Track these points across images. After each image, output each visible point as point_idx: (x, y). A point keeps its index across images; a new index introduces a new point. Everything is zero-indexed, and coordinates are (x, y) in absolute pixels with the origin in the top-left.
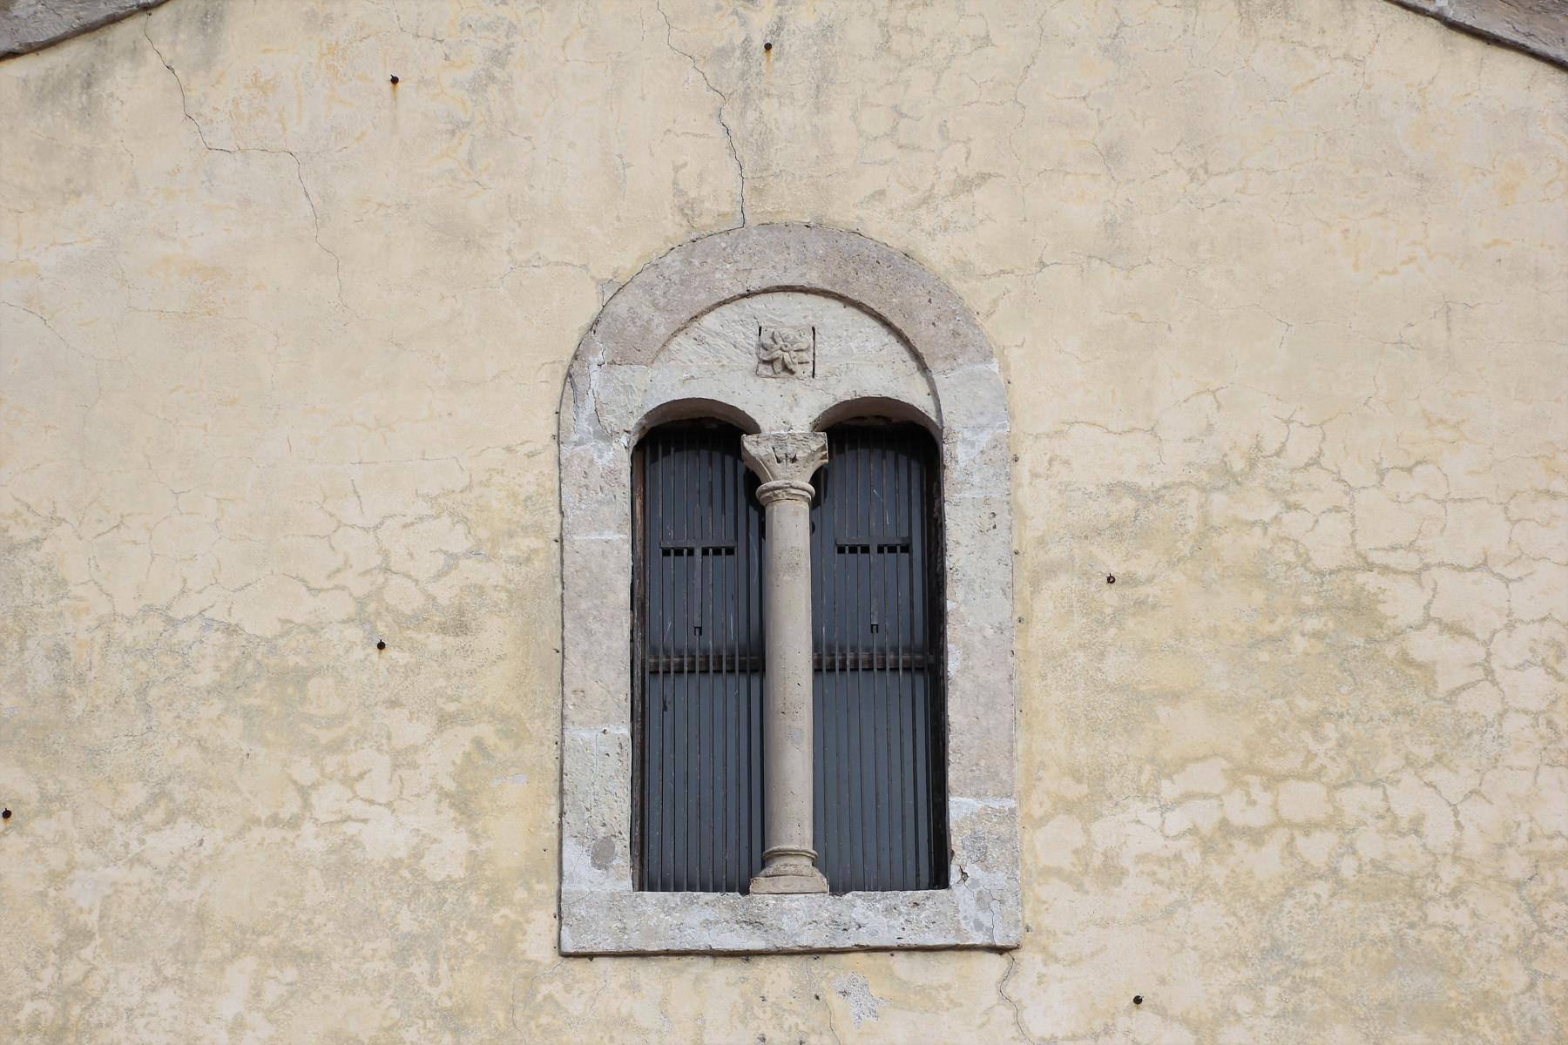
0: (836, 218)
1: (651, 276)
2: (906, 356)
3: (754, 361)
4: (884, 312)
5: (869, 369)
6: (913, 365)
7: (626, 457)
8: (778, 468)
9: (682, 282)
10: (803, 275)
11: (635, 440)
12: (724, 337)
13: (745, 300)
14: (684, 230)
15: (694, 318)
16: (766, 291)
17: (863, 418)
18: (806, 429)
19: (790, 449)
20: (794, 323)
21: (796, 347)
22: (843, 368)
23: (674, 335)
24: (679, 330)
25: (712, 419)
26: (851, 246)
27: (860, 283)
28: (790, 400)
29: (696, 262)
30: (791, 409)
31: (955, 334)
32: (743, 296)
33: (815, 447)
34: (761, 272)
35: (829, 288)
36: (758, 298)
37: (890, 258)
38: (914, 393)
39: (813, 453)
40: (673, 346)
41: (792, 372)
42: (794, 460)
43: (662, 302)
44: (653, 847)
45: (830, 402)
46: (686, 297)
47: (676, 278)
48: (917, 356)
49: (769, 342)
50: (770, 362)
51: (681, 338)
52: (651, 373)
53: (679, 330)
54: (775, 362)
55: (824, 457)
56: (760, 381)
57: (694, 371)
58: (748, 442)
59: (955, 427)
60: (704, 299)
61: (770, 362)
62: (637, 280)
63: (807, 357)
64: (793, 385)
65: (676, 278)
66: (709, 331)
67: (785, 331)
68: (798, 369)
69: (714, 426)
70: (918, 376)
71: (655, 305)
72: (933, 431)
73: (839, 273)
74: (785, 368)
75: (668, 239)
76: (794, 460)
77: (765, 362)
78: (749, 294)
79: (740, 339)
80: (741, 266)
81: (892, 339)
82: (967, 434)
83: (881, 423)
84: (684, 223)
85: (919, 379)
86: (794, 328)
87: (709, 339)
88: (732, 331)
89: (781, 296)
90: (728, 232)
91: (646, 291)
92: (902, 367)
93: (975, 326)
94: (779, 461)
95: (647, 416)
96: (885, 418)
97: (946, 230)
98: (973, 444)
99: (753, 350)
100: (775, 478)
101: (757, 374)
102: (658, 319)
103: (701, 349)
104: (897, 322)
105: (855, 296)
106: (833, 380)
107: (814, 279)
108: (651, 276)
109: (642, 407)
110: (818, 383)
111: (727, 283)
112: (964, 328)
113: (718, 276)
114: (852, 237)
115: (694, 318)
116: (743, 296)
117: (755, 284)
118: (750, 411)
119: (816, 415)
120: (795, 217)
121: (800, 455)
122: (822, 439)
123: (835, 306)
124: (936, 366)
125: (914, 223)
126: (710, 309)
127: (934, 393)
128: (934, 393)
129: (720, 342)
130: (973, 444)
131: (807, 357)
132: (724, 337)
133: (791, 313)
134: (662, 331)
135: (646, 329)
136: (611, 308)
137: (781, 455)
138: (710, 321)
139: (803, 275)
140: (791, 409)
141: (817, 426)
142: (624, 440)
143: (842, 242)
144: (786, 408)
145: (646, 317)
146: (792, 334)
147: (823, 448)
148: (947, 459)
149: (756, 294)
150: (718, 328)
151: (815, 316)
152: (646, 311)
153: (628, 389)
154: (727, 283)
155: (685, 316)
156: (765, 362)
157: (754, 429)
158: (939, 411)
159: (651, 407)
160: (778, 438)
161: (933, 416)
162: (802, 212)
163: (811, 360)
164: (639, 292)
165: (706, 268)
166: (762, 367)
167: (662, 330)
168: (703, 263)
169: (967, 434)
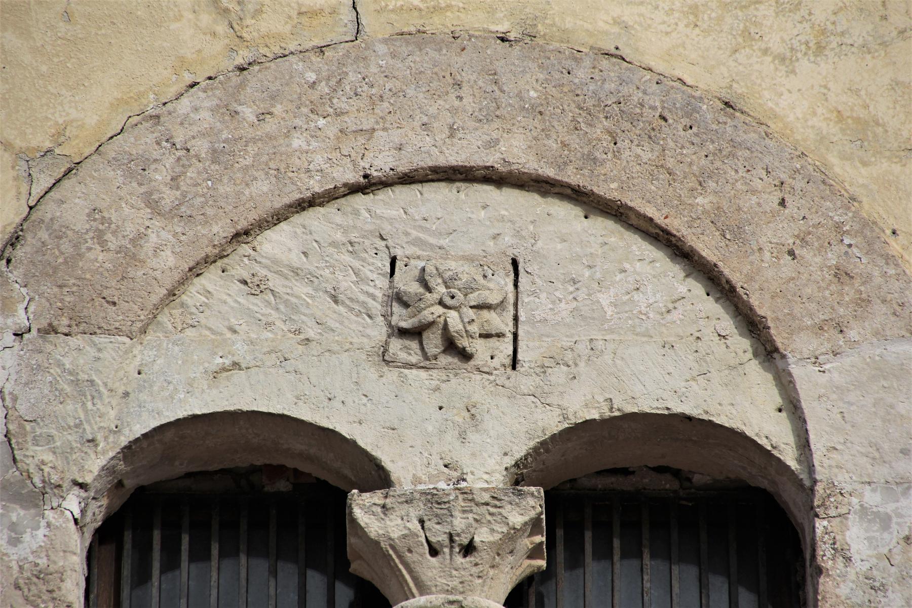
0: (569, 23)
1: (143, 141)
2: (728, 324)
3: (378, 332)
4: (677, 225)
5: (642, 352)
6: (742, 344)
7: (77, 545)
8: (431, 569)
9: (215, 155)
10: (492, 144)
11: (97, 513)
12: (310, 278)
13: (359, 200)
14: (219, 46)
15: (241, 236)
16: (408, 179)
17: (625, 472)
18: (498, 479)
19: (459, 523)
20: (469, 248)
21: (474, 298)
22: (583, 348)
23: (195, 271)
24: (208, 261)
25: (277, 471)
26: (606, 84)
27: (616, 167)
28: (461, 417)
29: (248, 113)
30: (462, 437)
31: (842, 275)
32: (355, 189)
33: (517, 519)
34: (396, 136)
35: (550, 172)
36: (384, 195)
37: (690, 109)
38: (747, 407)
39: (513, 534)
40: (192, 295)
41: (465, 356)
42: (469, 549)
43: (169, 197)
44: (92, 596)
45: (552, 423)
46: (225, 188)
47: (201, 146)
48: (752, 324)
49: (415, 288)
50: (415, 333)
51: (210, 279)
52: (141, 354)
53: (208, 261)
54: (426, 332)
55: (534, 553)
56: (392, 375)
57: (240, 351)
58: (364, 509)
59: (842, 479)
60: (265, 193)
61: (415, 333)
62: (110, 150)
63: (501, 322)
64: (466, 385)
65: (201, 146)
66: (275, 265)
67: (452, 266)
68: (479, 348)
69: (283, 486)
70: (755, 371)
71: (152, 203)
72: (789, 496)
73: (574, 140)
74: (451, 346)
75: (182, 63)
76: (469, 549)
77: (403, 333)
78: (368, 185)
79: (346, 283)
80: (350, 122)
81: (696, 289)
82: (872, 498)
83: (667, 484)
84: (221, 28)
85: (759, 383)
86: (469, 259)
87: (275, 282)
88: (330, 264)
89: (438, 195)
90: (321, 50)
91: (130, 174)
92: (718, 347)
93: (889, 259)
94: (434, 551)
95: (130, 451)
96: (677, 473)
97: (820, 49)
98: (885, 522)
99: (377, 307)
100: (423, 589)
101: (385, 359)
102: (159, 233)
103: (257, 305)
104: (707, 247)
105: (609, 190)
106: (558, 375)
107: (517, 151)
108: (143, 141)
109: (118, 430)
110: (524, 380)
111: (319, 160)
112: (861, 264)
113: (298, 142)
114: (605, 63)
115: (241, 236)
116: (355, 189)
117: (382, 162)
118: (366, 439)
119: (520, 450)
120: (475, 21)
121: (482, 536)
122: (531, 505)
123: (565, 213)
124: (797, 347)
125: (747, 34)
126: (278, 217)
127: (793, 407)
128: (793, 407)
129: (302, 289)
130: (885, 522)
131: (501, 322)
132: (310, 278)
133: (465, 228)
134: (167, 262)
135: (130, 255)
136: (48, 209)
137: (439, 535)
138: (278, 243)
139: (492, 144)
140: (462, 437)
141: (520, 477)
142: (73, 503)
143: (581, 74)
144: (451, 436)
145: (130, 229)
146: (466, 272)
147: (534, 526)
148: (825, 554)
149: (384, 184)
150: (296, 259)
151: (518, 234)
152: (131, 217)
153: (84, 388)
154: (319, 160)
155: (221, 230)
156: (403, 333)
157: (377, 477)
158: (804, 445)
159: (139, 429)
160: (433, 499)
161: (790, 458)
162: (491, 11)
163: (508, 329)
164: (116, 176)
165: (270, 126)
166: (396, 345)
167: (168, 259)
168: (262, 116)
169: (872, 498)
